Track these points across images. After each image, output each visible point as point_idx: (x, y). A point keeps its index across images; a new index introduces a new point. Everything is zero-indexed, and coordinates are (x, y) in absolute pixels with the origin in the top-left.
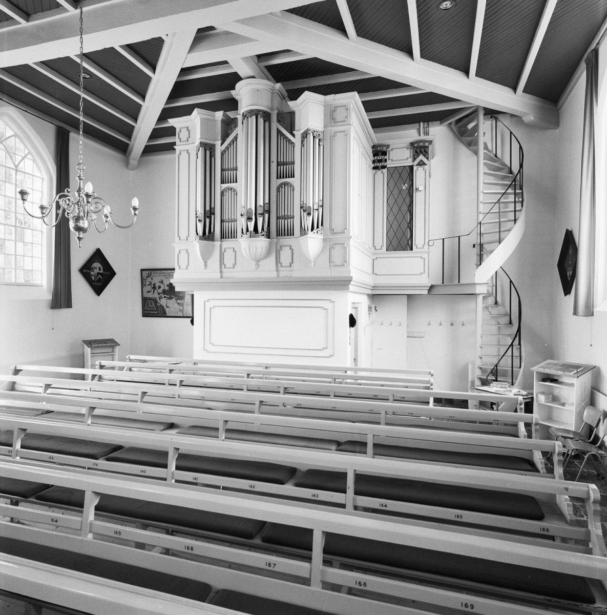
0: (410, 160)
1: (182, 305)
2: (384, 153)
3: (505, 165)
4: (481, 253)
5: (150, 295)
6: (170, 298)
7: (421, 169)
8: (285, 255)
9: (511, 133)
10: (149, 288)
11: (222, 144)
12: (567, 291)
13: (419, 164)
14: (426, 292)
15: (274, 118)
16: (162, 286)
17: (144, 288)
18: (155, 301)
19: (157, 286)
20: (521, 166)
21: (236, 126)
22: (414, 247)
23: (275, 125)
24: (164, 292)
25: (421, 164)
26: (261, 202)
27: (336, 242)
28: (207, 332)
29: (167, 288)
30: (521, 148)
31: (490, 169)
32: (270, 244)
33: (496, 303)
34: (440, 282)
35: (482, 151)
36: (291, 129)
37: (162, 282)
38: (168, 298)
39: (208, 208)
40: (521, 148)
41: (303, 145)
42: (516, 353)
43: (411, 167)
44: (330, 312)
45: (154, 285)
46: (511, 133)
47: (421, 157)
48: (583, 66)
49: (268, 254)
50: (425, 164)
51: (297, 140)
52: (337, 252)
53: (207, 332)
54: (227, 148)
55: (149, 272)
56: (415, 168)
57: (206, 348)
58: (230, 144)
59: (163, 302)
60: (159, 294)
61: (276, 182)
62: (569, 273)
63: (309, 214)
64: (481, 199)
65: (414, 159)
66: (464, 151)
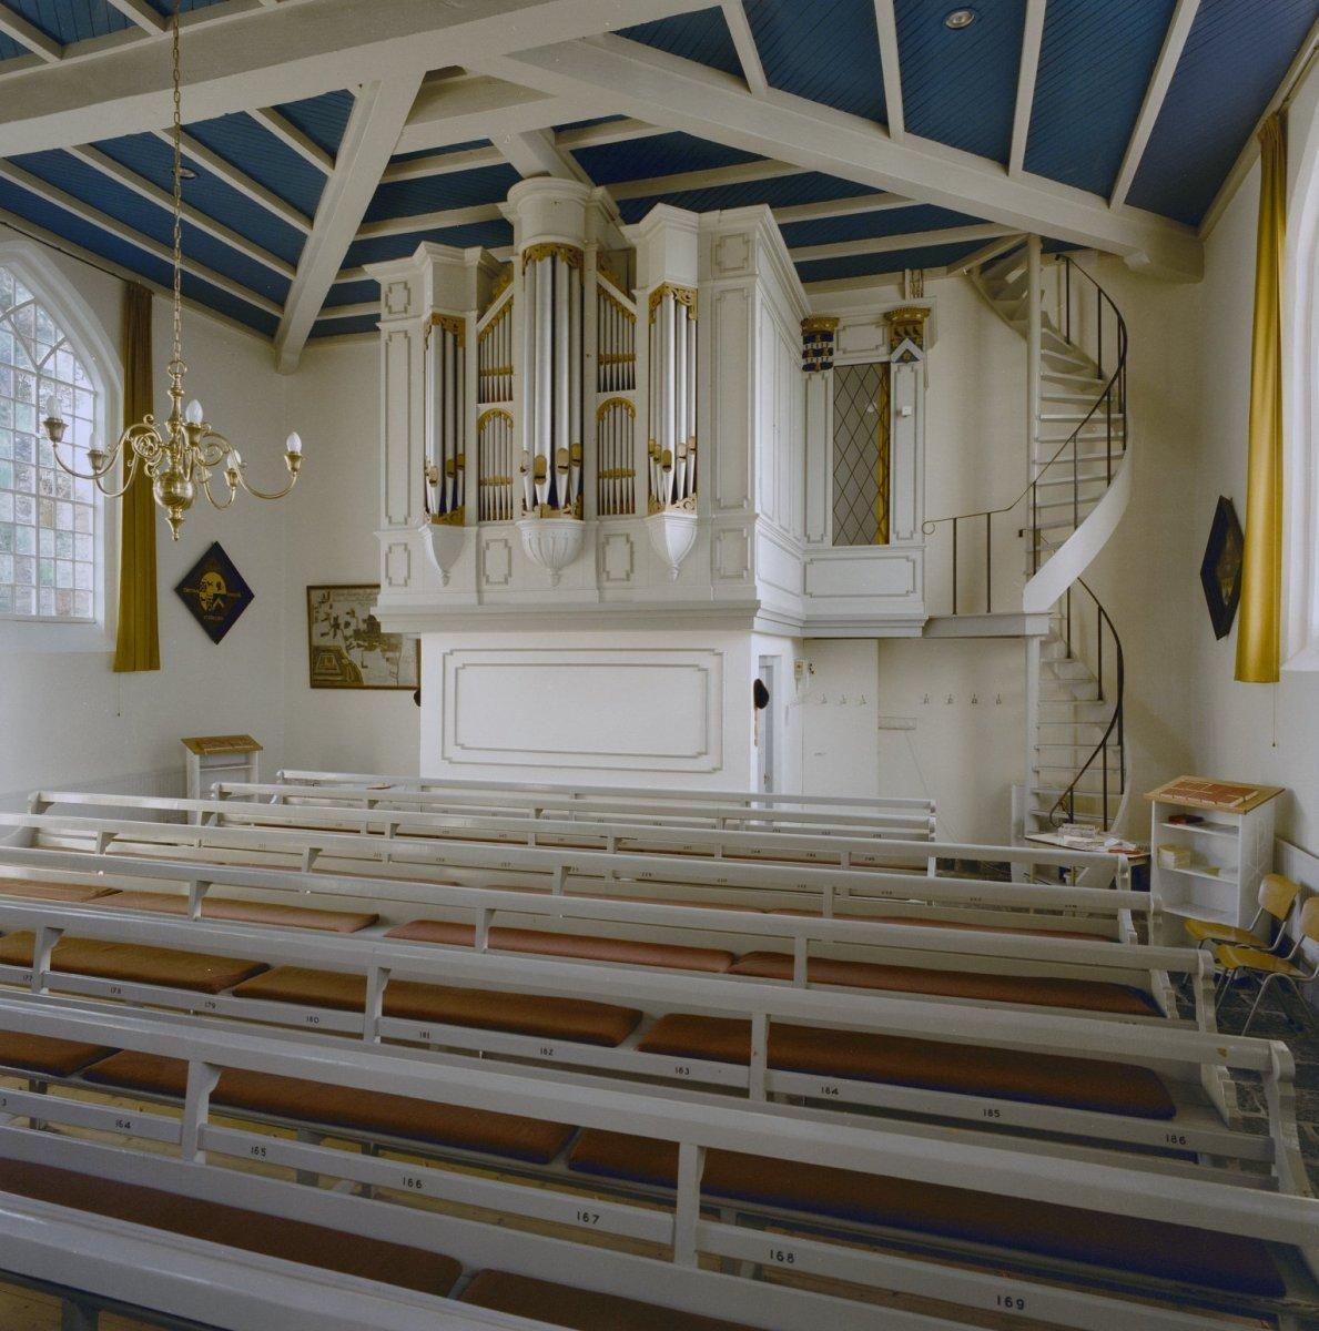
2: (828, 337)
3: (1086, 359)
4: (1037, 548)
5: (327, 642)
6: (371, 648)
7: (906, 369)
9: (1100, 291)
10: (325, 626)
11: (479, 318)
12: (1222, 629)
13: (902, 360)
14: (919, 633)
15: (591, 261)
16: (353, 622)
19: (341, 621)
22: (892, 537)
23: (593, 276)
24: (357, 633)
25: (908, 358)
29: (363, 627)
30: (1121, 323)
35: (1037, 331)
37: (352, 613)
38: (366, 649)
39: (450, 456)
41: (652, 320)
42: (1113, 761)
43: (886, 366)
45: (336, 619)
46: (1100, 291)
47: (907, 344)
51: (640, 310)
54: (491, 326)
56: (894, 367)
58: (496, 319)
59: (355, 656)
60: (346, 638)
61: (595, 399)
62: (1227, 590)
64: (1036, 432)
65: (892, 349)
66: (999, 331)
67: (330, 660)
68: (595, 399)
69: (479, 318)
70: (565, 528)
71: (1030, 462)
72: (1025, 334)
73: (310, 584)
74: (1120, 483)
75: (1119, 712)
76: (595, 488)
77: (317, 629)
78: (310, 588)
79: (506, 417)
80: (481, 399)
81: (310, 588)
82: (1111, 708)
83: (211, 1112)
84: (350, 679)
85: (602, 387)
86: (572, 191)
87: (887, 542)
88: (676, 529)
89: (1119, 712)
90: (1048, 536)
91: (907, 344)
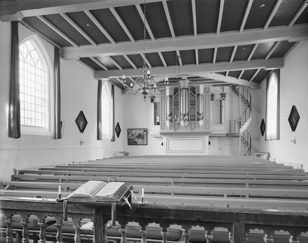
0: (221, 98)
1: (143, 141)
2: (213, 96)
3: (246, 99)
4: (240, 125)
5: (131, 138)
6: (139, 139)
7: (224, 101)
8: (193, 127)
9: (248, 91)
10: (131, 135)
11: (174, 95)
12: (263, 135)
13: (223, 100)
14: (225, 136)
15: (189, 89)
16: (136, 134)
17: (129, 135)
18: (133, 140)
19: (134, 134)
20: (251, 102)
21: (178, 91)
22: (222, 123)
23: (190, 91)
24: (137, 136)
25: (224, 99)
26: (187, 112)
27: (207, 123)
28: (168, 147)
29: (138, 135)
30: (250, 95)
31: (244, 104)
32: (189, 123)
33: (244, 139)
34: (230, 133)
35: (240, 96)
36: (194, 93)
37: (136, 133)
38: (138, 139)
39: (171, 113)
40: (250, 95)
41: (198, 97)
42: (250, 152)
43: (221, 100)
44: (204, 141)
45: (133, 134)
46: (248, 91)
47: (224, 98)
48: (265, 80)
49: (188, 126)
50: (225, 99)
51: (196, 96)
52: (207, 125)
53: (168, 147)
54: (176, 96)
55: (131, 130)
56: (222, 100)
57: (167, 152)
58: (176, 96)
59: (136, 140)
60: (134, 137)
61: (190, 107)
62: (263, 130)
63: (200, 115)
64: (240, 109)
65: (222, 98)
66: (234, 95)
67: (131, 141)
68: (190, 107)
69: (174, 95)
70: (187, 123)
71: (239, 113)
72: (238, 95)
73: (129, 128)
74: (251, 117)
75: (250, 146)
76: (194, 117)
77: (129, 136)
78: (128, 129)
79: (178, 108)
80: (174, 106)
81: (147, 129)
82: (249, 146)
83: (144, 195)
84: (135, 144)
85: (191, 105)
86: (187, 81)
87: (221, 124)
88: (201, 122)
89: (250, 146)
90: (242, 123)
91: (224, 98)
